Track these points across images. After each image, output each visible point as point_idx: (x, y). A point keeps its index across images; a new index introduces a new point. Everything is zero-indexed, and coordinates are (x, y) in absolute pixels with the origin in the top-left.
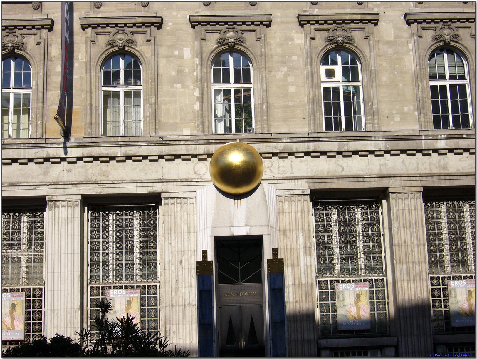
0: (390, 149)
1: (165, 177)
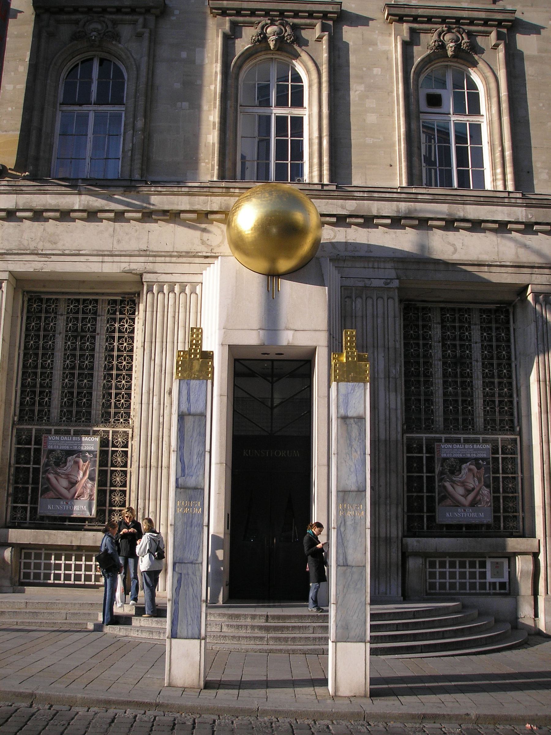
0: (533, 220)
1: (151, 248)
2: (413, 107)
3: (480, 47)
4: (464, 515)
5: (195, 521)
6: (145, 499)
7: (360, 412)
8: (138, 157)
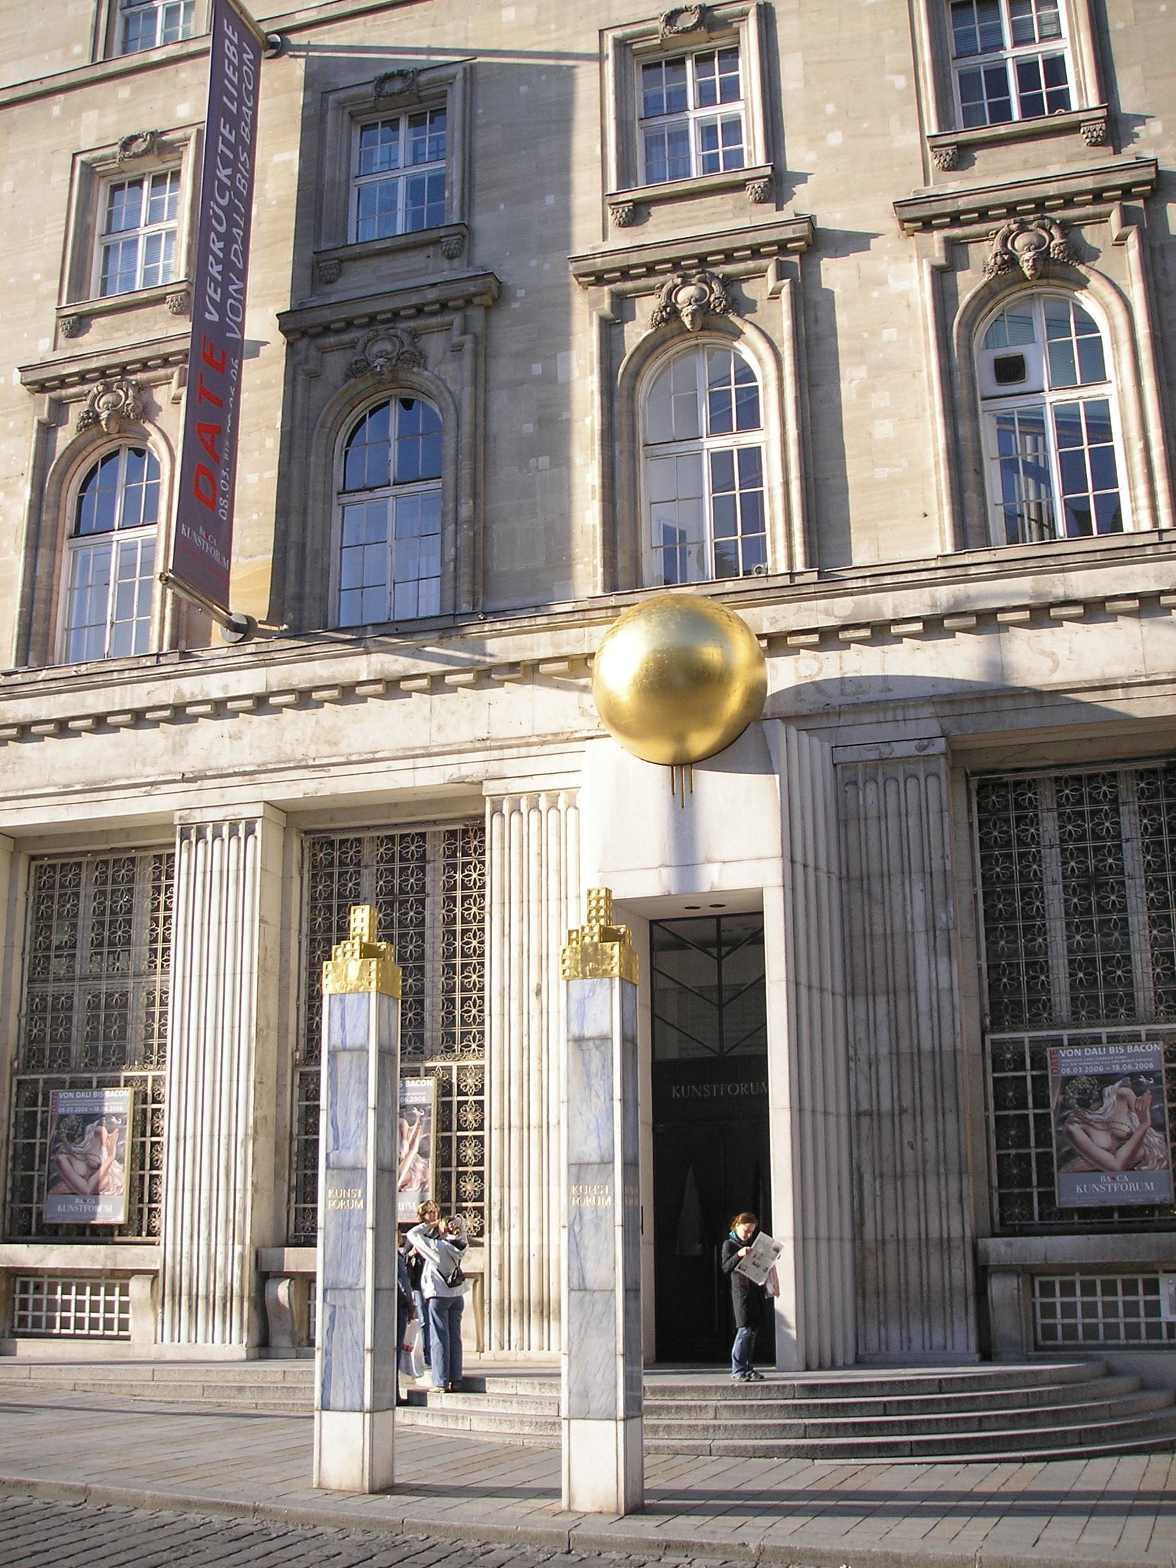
1: (493, 735)
2: (961, 394)
3: (1090, 247)
4: (1113, 1188)
5: (354, 1222)
6: (502, 1186)
7: (604, 1028)
8: (464, 570)
